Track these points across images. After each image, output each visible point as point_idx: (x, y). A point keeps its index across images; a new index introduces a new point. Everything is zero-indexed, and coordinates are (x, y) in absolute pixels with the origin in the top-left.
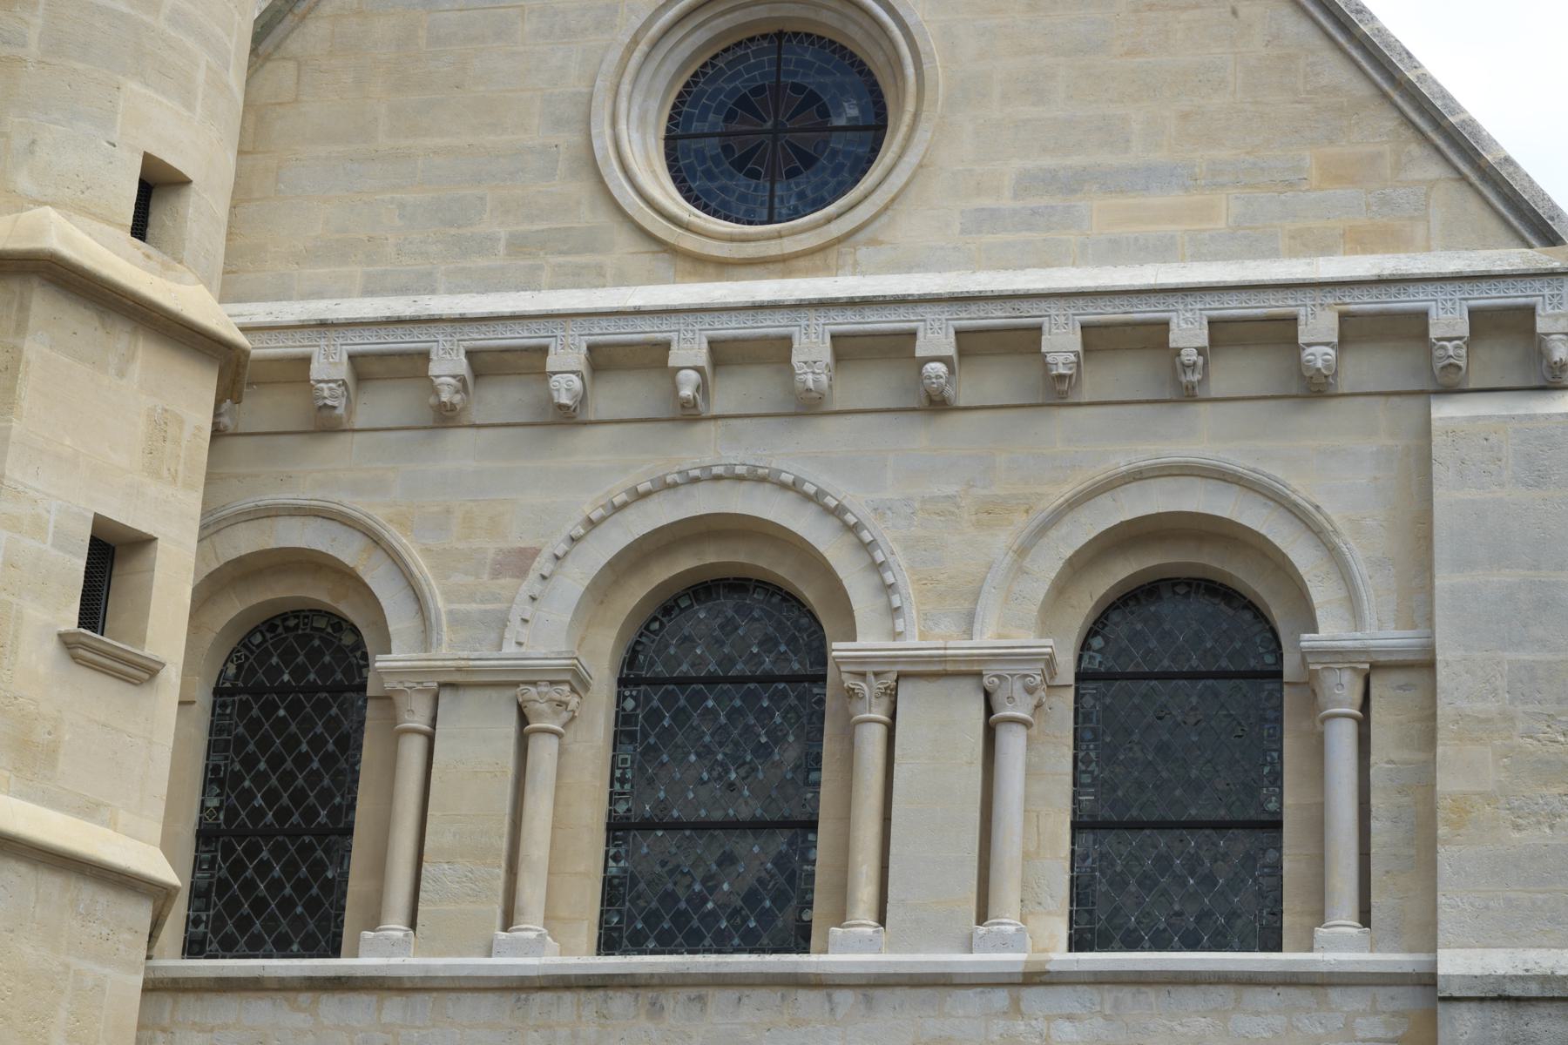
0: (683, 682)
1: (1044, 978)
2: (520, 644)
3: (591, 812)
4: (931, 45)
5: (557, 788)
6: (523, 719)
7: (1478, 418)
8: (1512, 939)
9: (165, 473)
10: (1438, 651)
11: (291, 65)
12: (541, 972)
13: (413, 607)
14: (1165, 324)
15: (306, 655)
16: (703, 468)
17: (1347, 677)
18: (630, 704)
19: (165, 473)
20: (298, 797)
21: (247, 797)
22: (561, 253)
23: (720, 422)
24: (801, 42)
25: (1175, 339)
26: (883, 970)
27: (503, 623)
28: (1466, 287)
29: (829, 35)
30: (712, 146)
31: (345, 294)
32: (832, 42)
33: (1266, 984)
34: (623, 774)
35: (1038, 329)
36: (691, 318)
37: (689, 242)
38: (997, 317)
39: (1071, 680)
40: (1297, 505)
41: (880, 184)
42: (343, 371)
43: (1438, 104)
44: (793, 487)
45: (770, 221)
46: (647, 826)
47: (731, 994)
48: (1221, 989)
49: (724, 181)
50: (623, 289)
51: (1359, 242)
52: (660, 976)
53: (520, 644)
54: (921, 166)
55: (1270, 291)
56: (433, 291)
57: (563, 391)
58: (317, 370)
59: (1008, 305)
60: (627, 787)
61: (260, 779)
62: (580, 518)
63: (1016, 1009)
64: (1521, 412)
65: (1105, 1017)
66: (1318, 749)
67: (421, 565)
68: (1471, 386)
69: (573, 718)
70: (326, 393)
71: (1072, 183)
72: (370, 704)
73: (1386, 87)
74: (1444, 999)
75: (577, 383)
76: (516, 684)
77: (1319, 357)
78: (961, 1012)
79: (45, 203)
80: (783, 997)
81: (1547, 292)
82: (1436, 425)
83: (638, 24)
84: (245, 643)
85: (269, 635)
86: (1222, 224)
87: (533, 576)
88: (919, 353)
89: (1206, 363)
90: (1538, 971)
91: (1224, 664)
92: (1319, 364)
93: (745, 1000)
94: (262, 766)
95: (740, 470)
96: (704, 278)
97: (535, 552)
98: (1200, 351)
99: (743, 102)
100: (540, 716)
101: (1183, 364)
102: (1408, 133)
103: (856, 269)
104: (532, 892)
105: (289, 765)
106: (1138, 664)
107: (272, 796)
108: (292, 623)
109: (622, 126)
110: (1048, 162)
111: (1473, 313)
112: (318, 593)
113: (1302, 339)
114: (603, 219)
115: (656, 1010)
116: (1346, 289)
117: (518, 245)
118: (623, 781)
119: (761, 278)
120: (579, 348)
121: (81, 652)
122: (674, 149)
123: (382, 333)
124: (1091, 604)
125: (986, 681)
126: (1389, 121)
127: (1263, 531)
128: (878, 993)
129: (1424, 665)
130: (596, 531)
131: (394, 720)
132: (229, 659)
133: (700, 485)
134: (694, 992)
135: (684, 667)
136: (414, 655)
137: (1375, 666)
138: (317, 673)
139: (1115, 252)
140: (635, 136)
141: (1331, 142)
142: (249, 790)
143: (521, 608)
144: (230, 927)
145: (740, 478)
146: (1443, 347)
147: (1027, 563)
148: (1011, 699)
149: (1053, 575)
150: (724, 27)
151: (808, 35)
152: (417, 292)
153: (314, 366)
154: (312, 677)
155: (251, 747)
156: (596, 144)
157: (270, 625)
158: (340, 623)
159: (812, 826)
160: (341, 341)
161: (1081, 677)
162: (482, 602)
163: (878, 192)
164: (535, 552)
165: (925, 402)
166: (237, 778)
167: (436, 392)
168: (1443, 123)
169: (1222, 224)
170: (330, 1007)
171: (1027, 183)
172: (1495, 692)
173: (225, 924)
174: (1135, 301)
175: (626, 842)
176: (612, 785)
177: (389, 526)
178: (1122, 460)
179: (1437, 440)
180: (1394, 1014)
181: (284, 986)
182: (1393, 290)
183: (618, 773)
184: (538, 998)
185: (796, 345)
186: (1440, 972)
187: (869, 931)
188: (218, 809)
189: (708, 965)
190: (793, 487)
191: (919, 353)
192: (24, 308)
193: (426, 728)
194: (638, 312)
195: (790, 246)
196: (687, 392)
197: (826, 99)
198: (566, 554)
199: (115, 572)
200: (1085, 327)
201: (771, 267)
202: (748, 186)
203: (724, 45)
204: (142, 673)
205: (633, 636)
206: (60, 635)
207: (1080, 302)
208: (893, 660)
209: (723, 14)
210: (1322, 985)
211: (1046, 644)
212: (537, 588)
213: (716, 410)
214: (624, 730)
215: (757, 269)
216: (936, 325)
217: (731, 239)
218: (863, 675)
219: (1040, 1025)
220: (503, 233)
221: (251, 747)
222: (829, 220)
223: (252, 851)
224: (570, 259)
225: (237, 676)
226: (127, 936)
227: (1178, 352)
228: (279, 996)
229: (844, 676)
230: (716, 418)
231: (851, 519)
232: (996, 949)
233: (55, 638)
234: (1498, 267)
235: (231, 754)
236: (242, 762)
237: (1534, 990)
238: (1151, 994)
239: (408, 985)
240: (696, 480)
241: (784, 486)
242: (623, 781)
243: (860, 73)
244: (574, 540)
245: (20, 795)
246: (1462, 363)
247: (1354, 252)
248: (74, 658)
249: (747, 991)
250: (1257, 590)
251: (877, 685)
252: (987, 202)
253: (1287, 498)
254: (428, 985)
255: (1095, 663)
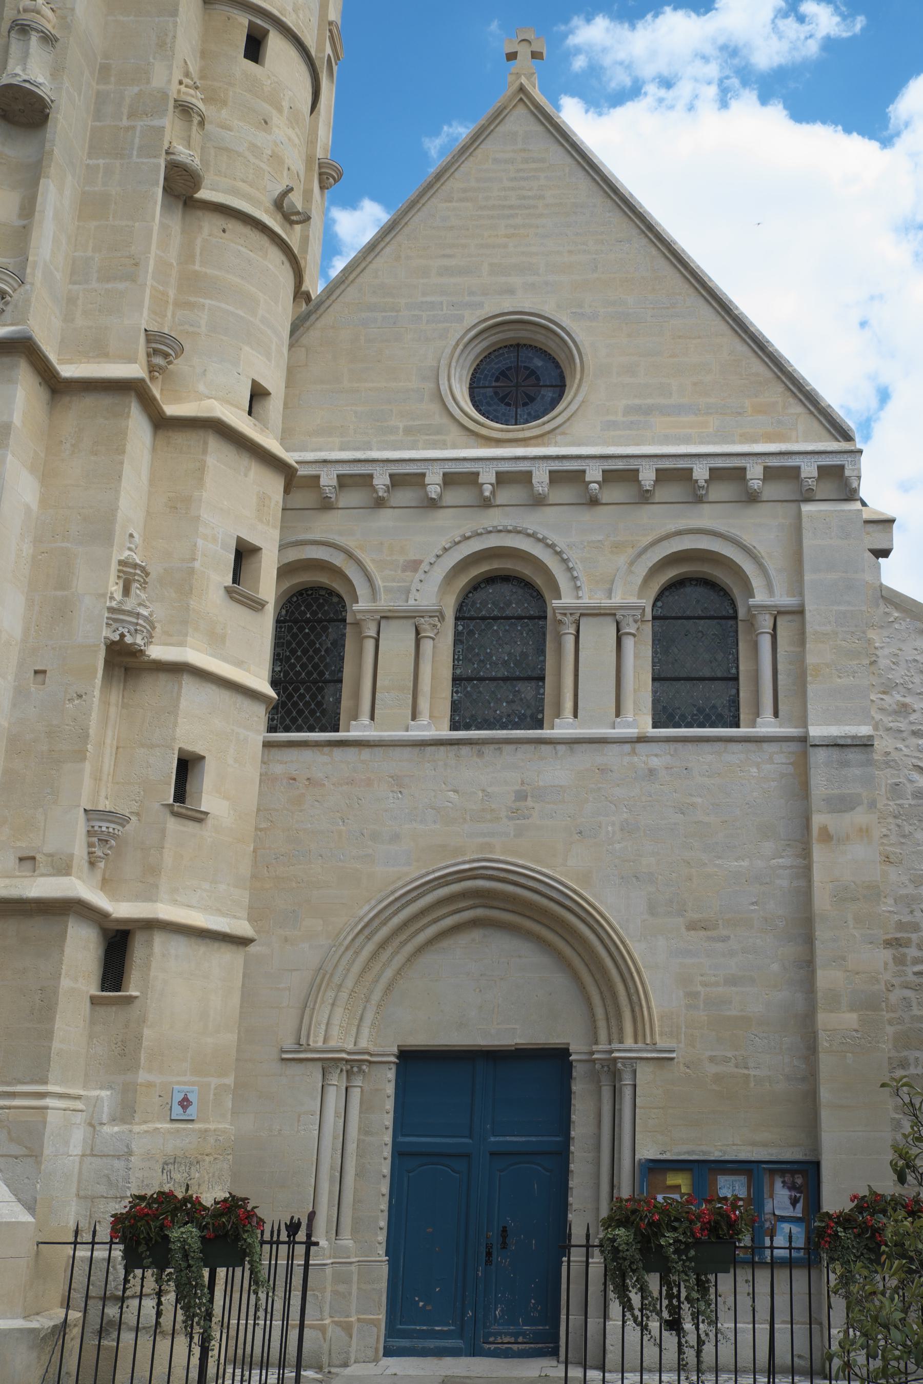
0: (483, 618)
1: (646, 739)
2: (416, 600)
3: (447, 674)
4: (586, 348)
5: (433, 662)
6: (418, 633)
7: (821, 511)
8: (838, 722)
9: (265, 520)
10: (806, 606)
11: (303, 349)
12: (431, 738)
13: (368, 584)
14: (691, 470)
15: (317, 607)
16: (494, 527)
17: (767, 617)
18: (460, 628)
19: (265, 520)
20: (316, 667)
21: (292, 666)
22: (427, 435)
23: (500, 508)
24: (527, 348)
25: (696, 475)
26: (578, 736)
27: (408, 591)
28: (816, 456)
29: (539, 345)
30: (489, 392)
31: (331, 450)
32: (541, 349)
33: (737, 741)
34: (459, 657)
35: (638, 470)
36: (488, 463)
37: (484, 431)
38: (620, 465)
39: (650, 618)
40: (746, 546)
41: (565, 409)
42: (334, 482)
43: (801, 381)
44: (533, 536)
45: (516, 424)
46: (469, 679)
47: (512, 747)
48: (719, 744)
49: (495, 407)
50: (456, 450)
51: (769, 438)
52: (482, 739)
53: (416, 600)
54: (583, 402)
55: (735, 457)
56: (371, 450)
57: (433, 492)
58: (323, 481)
59: (625, 460)
60: (461, 662)
61: (298, 659)
62: (440, 547)
63: (634, 752)
64: (839, 509)
65: (671, 755)
66: (755, 647)
67: (371, 567)
68: (817, 498)
69: (438, 633)
70: (327, 491)
71: (648, 411)
72: (348, 627)
73: (779, 374)
74: (812, 746)
75: (439, 489)
76: (415, 617)
77: (756, 484)
78: (611, 754)
79: (212, 398)
80: (535, 748)
81: (849, 459)
82: (803, 513)
83: (459, 337)
84: (289, 601)
85: (300, 598)
86: (711, 430)
87: (421, 571)
88: (587, 479)
89: (708, 486)
90: (851, 734)
91: (712, 613)
92: (756, 487)
93: (519, 749)
94: (299, 653)
95: (510, 528)
96: (490, 447)
97: (421, 562)
98: (706, 481)
99: (503, 373)
100: (425, 631)
101: (699, 486)
102: (789, 394)
103: (556, 444)
104: (424, 705)
105: (311, 653)
106: (676, 613)
107: (303, 666)
108: (310, 592)
109: (453, 381)
110: (637, 401)
111: (819, 467)
112: (323, 579)
113: (748, 477)
114: (445, 420)
115: (480, 754)
116: (766, 456)
117: (408, 431)
118: (458, 660)
119: (516, 447)
120: (439, 474)
121: (234, 595)
122: (473, 392)
123: (352, 466)
124: (658, 587)
125: (617, 617)
126: (780, 388)
127: (731, 557)
128: (576, 746)
129: (800, 612)
130: (447, 553)
131: (361, 633)
132: (282, 608)
133: (492, 534)
134: (497, 746)
135: (483, 613)
136: (370, 604)
137: (779, 613)
138: (322, 614)
139: (666, 440)
140: (458, 386)
141: (756, 397)
142: (294, 664)
143: (416, 585)
144: (288, 721)
145: (509, 532)
146: (807, 481)
147: (633, 569)
148: (628, 625)
149: (644, 574)
150: (495, 340)
151: (531, 346)
152: (364, 450)
153: (321, 479)
154: (320, 615)
155: (294, 645)
156: (442, 388)
157: (300, 593)
158: (331, 592)
159: (542, 679)
160: (333, 469)
161: (654, 618)
162: (398, 582)
163: (565, 412)
164: (421, 562)
165: (589, 500)
166: (288, 658)
167: (376, 491)
168: (804, 390)
169: (711, 430)
170: (338, 752)
171: (628, 410)
172: (830, 622)
173: (285, 720)
174: (678, 459)
175: (460, 685)
176: (454, 662)
177: (356, 550)
178: (672, 527)
179: (804, 520)
180: (789, 753)
181: (317, 744)
182: (786, 457)
183: (456, 657)
184: (429, 749)
185: (534, 475)
186: (811, 735)
187: (571, 720)
188: (280, 672)
189: (503, 734)
190: (533, 536)
191: (587, 479)
192: (206, 443)
193: (375, 636)
194: (465, 459)
195: (528, 434)
196: (487, 494)
197: (539, 373)
198: (435, 562)
199: (243, 563)
200: (657, 470)
201: (519, 443)
202: (506, 410)
203: (494, 349)
204: (256, 605)
205: (461, 599)
206: (225, 587)
207: (655, 460)
208: (578, 608)
209: (495, 334)
210: (760, 742)
211: (643, 602)
212: (423, 577)
213: (498, 503)
214: (458, 639)
215: (513, 444)
216: (594, 468)
217: (502, 430)
218: (565, 614)
219: (644, 758)
220: (401, 425)
221: (294, 645)
222: (544, 424)
223: (296, 690)
224: (431, 437)
225: (286, 615)
226: (256, 719)
227: (696, 481)
228: (315, 749)
229: (557, 615)
230: (498, 506)
231: (558, 549)
232: (624, 727)
233: (223, 589)
234: (829, 449)
235: (285, 648)
236: (290, 652)
237: (849, 742)
238: (690, 746)
239: (372, 744)
240: (490, 532)
241: (529, 535)
242: (458, 660)
243: (553, 362)
244: (438, 556)
245: (212, 656)
246: (814, 488)
247: (766, 442)
248: (231, 598)
249: (519, 746)
250: (728, 582)
251: (572, 619)
252: (612, 418)
253: (742, 543)
254: (382, 743)
255: (659, 612)
